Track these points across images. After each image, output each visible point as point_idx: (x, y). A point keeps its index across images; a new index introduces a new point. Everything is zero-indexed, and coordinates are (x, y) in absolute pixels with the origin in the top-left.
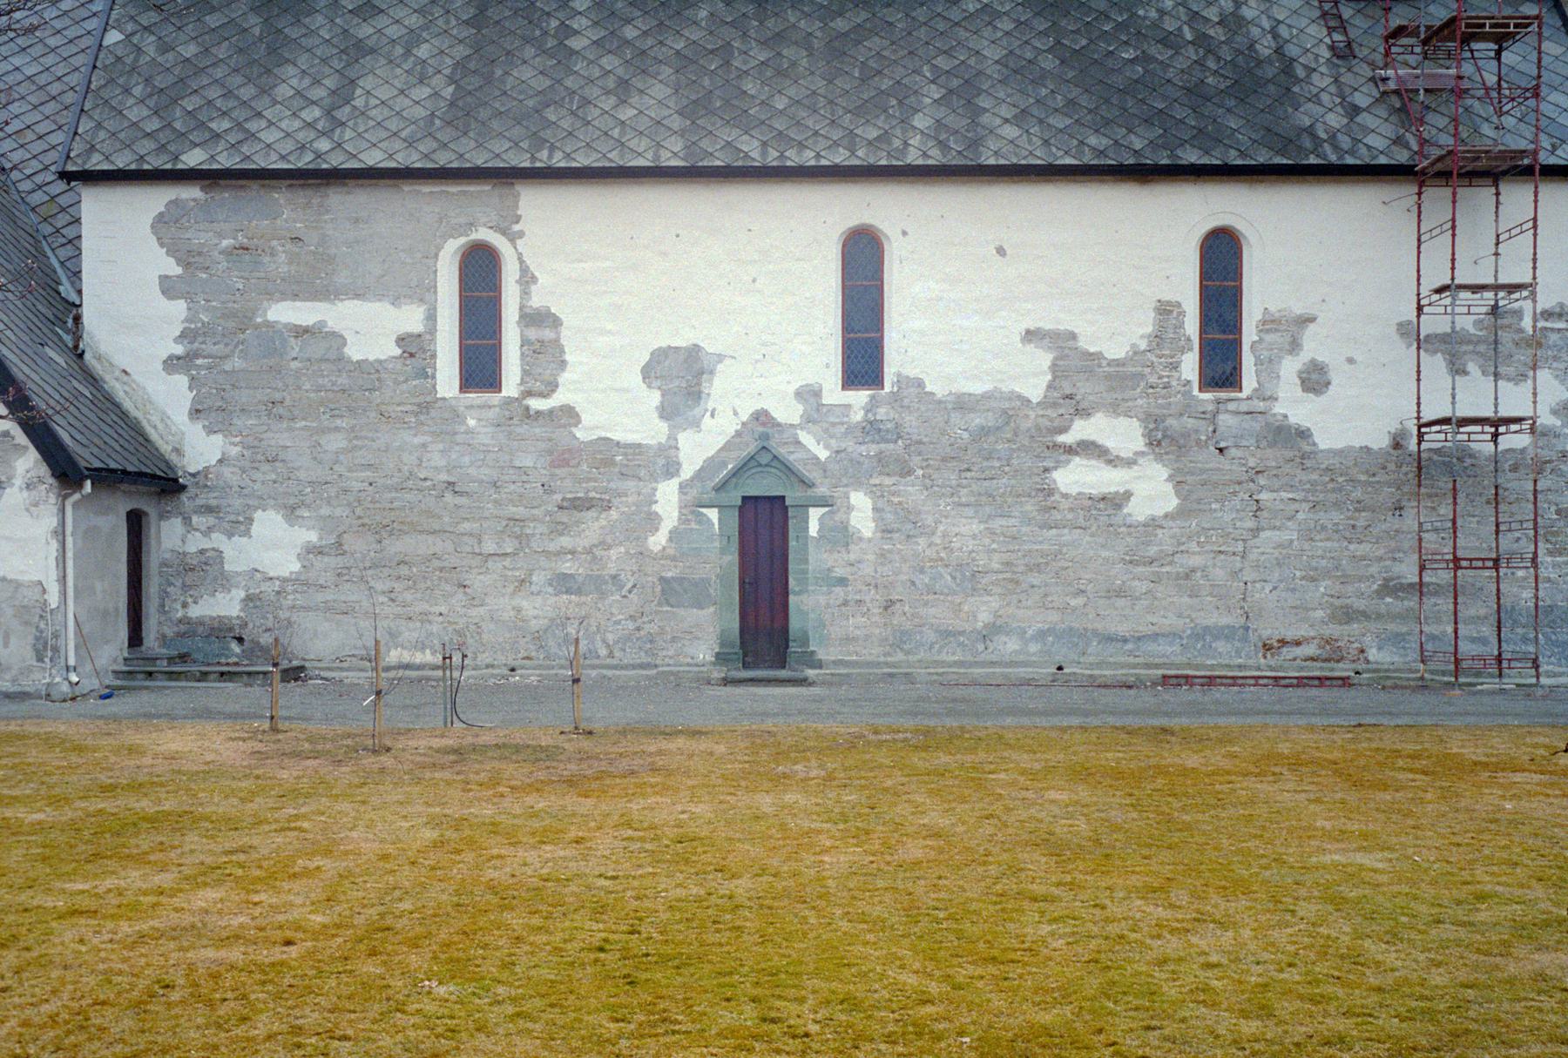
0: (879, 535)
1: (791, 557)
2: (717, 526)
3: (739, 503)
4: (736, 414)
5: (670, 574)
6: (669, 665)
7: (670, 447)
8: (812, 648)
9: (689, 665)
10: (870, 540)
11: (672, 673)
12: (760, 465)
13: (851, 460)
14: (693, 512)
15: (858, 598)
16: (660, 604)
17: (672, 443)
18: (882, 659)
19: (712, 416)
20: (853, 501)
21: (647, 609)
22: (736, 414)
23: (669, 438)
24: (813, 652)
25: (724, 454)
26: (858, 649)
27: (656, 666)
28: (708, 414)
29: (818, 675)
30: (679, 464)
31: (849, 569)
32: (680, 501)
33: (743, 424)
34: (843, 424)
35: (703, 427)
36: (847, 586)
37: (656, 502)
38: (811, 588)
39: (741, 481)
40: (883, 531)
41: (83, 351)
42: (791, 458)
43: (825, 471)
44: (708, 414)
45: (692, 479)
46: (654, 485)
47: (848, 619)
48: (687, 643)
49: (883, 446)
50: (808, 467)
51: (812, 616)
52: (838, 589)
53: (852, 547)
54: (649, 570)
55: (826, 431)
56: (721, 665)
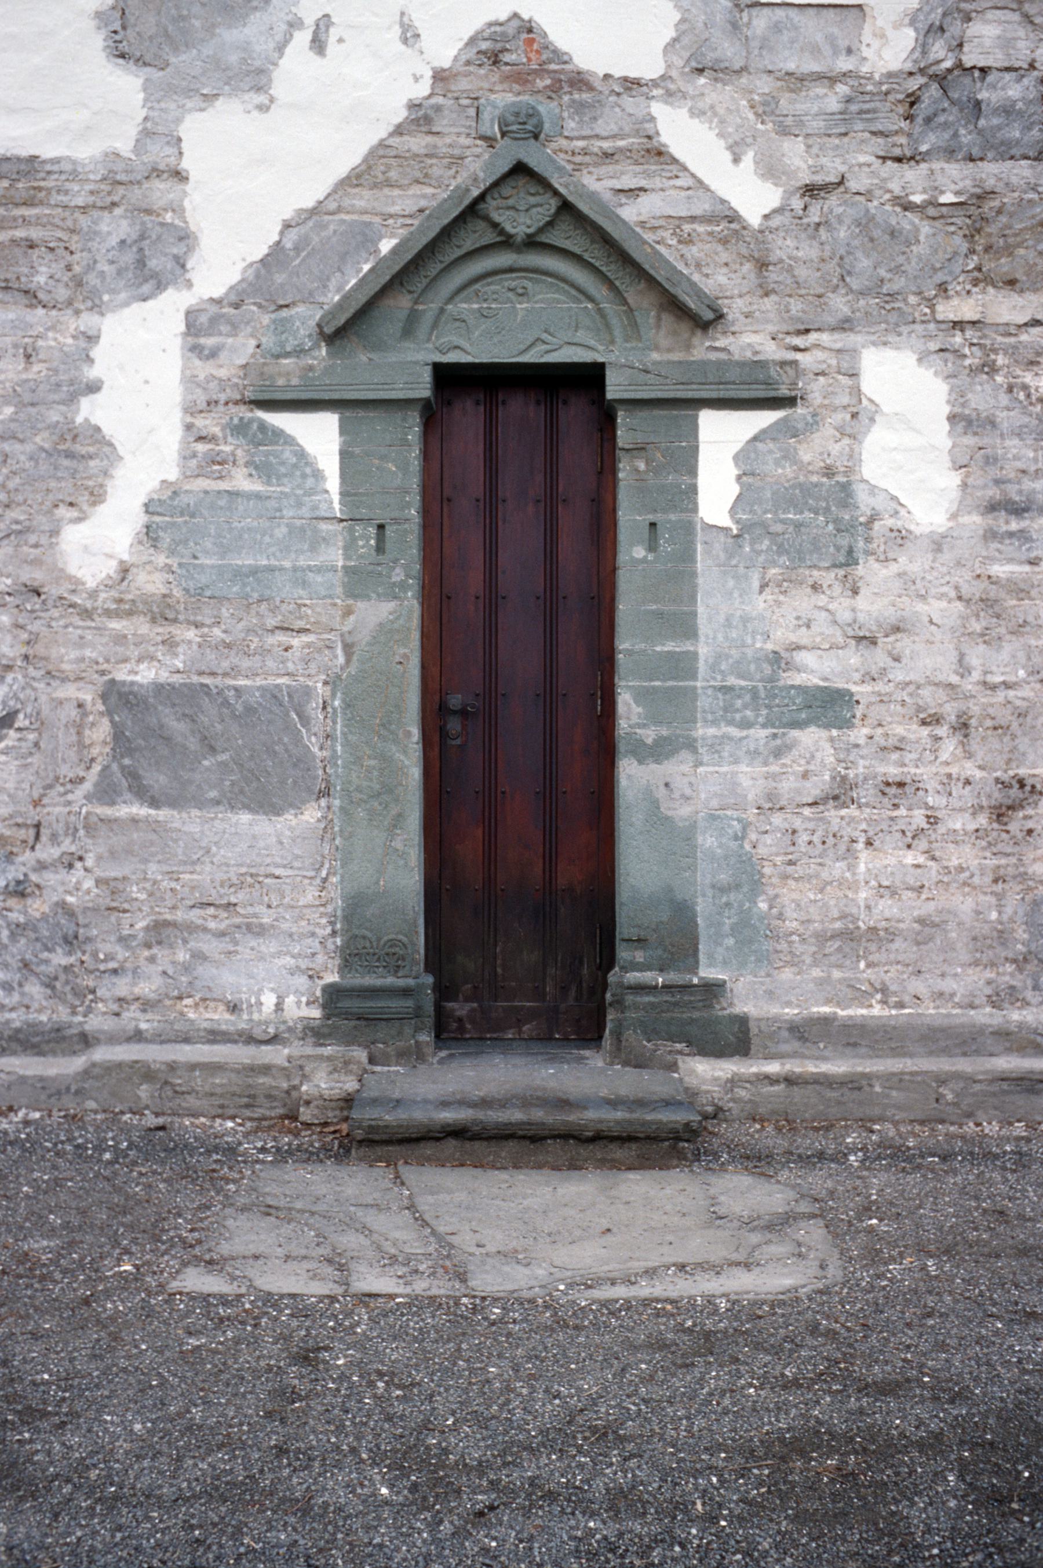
0: (975, 520)
1: (624, 608)
2: (333, 484)
3: (424, 389)
4: (409, 36)
5: (146, 675)
6: (138, 1037)
7: (155, 172)
8: (708, 972)
9: (215, 1036)
10: (938, 544)
11: (146, 1073)
12: (506, 242)
13: (865, 224)
14: (240, 429)
15: (893, 772)
16: (106, 793)
17: (159, 153)
18: (985, 1016)
19: (318, 45)
20: (868, 385)
21: (55, 811)
22: (409, 36)
23: (147, 133)
24: (713, 990)
25: (362, 199)
26: (890, 975)
27: (86, 1041)
28: (302, 38)
29: (733, 1082)
30: (186, 238)
31: (854, 658)
32: (189, 380)
33: (440, 77)
34: (831, 79)
35: (279, 88)
36: (846, 724)
37: (94, 388)
38: (703, 731)
39: (429, 308)
40: (992, 507)
41: (736, 160)
42: (630, 212)
43: (762, 265)
44: (302, 38)
45: (237, 298)
46: (88, 321)
47: (850, 853)
48: (210, 946)
49: (991, 171)
50: (694, 251)
51: (707, 841)
52: (810, 737)
53: (868, 569)
54: (67, 657)
55: (765, 109)
56: (349, 1040)
